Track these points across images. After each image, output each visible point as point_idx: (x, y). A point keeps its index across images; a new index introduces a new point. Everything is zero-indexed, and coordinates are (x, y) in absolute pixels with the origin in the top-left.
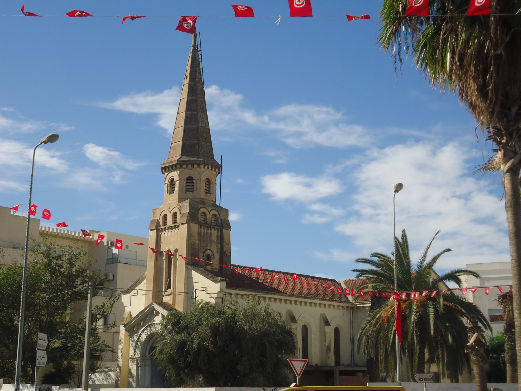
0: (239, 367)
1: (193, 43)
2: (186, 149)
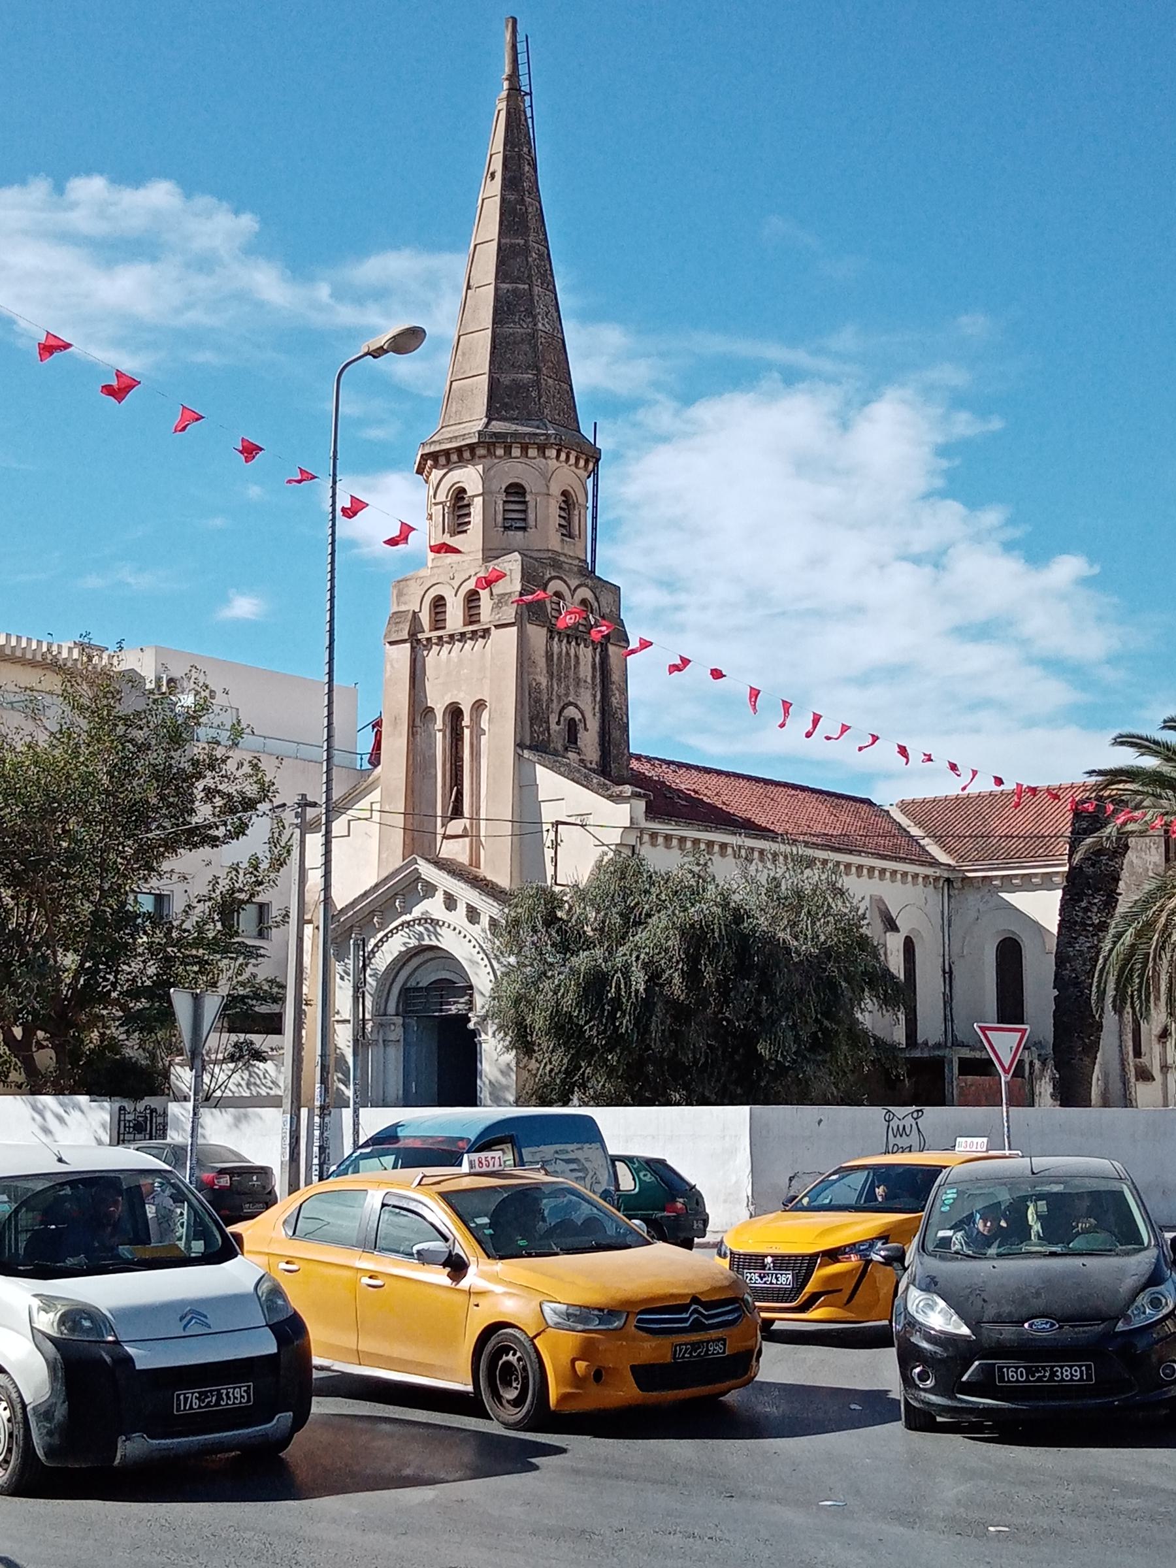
0: (763, 1049)
1: (507, 70)
2: (502, 399)
